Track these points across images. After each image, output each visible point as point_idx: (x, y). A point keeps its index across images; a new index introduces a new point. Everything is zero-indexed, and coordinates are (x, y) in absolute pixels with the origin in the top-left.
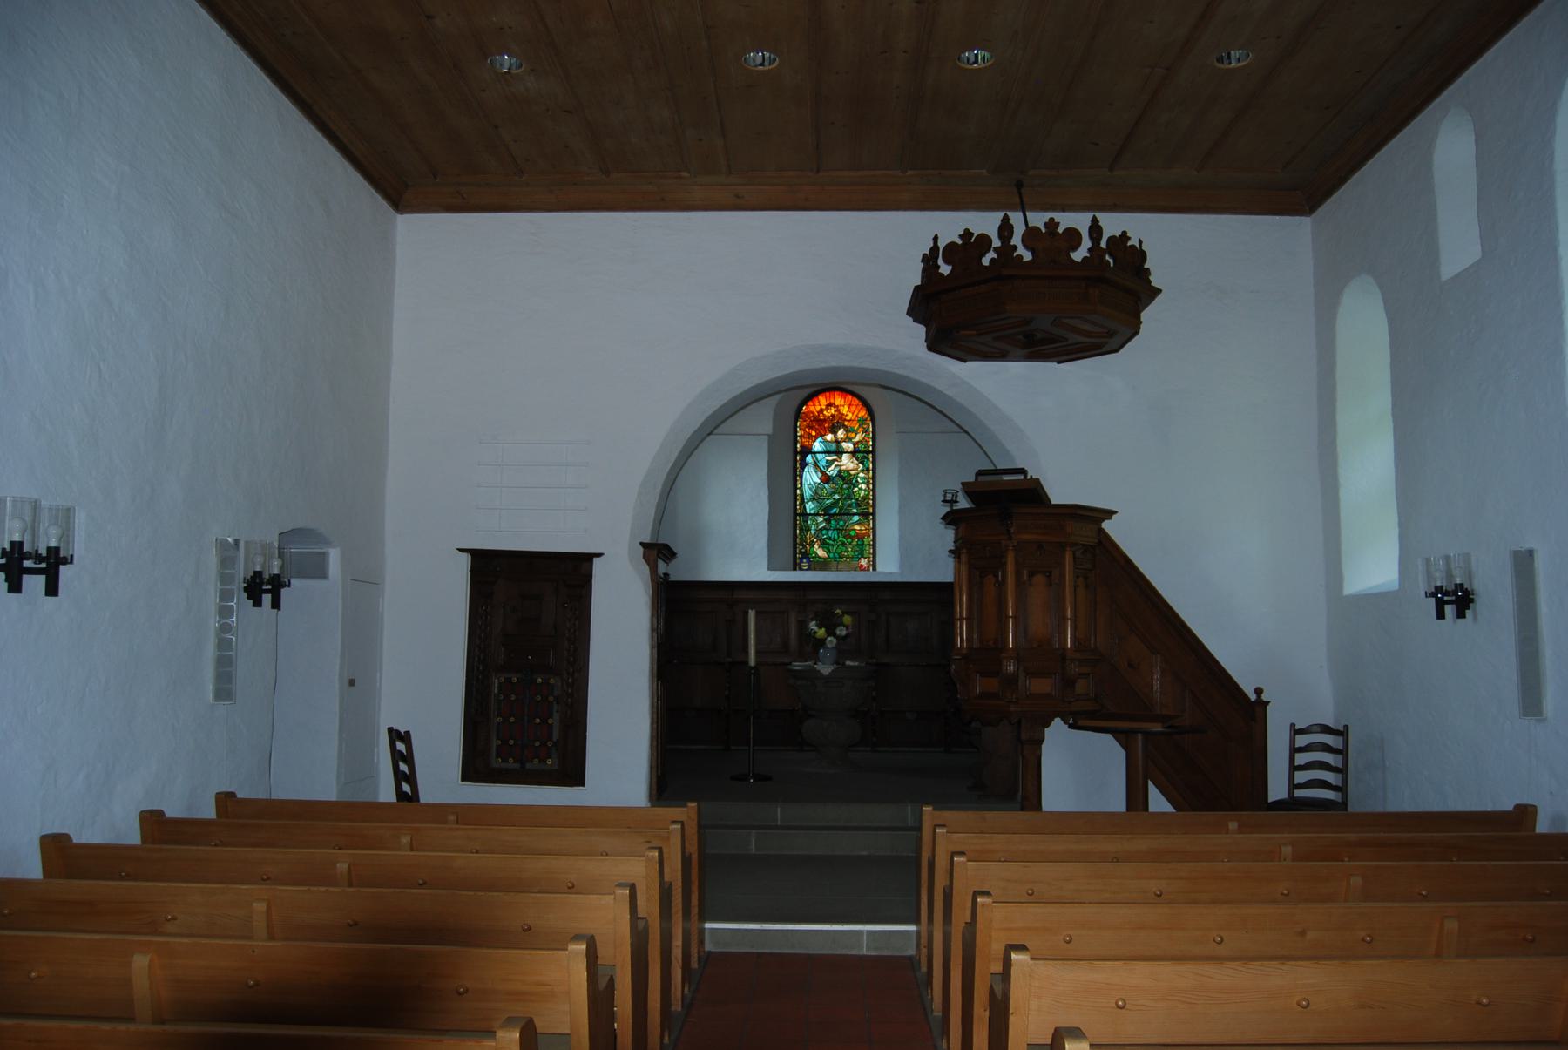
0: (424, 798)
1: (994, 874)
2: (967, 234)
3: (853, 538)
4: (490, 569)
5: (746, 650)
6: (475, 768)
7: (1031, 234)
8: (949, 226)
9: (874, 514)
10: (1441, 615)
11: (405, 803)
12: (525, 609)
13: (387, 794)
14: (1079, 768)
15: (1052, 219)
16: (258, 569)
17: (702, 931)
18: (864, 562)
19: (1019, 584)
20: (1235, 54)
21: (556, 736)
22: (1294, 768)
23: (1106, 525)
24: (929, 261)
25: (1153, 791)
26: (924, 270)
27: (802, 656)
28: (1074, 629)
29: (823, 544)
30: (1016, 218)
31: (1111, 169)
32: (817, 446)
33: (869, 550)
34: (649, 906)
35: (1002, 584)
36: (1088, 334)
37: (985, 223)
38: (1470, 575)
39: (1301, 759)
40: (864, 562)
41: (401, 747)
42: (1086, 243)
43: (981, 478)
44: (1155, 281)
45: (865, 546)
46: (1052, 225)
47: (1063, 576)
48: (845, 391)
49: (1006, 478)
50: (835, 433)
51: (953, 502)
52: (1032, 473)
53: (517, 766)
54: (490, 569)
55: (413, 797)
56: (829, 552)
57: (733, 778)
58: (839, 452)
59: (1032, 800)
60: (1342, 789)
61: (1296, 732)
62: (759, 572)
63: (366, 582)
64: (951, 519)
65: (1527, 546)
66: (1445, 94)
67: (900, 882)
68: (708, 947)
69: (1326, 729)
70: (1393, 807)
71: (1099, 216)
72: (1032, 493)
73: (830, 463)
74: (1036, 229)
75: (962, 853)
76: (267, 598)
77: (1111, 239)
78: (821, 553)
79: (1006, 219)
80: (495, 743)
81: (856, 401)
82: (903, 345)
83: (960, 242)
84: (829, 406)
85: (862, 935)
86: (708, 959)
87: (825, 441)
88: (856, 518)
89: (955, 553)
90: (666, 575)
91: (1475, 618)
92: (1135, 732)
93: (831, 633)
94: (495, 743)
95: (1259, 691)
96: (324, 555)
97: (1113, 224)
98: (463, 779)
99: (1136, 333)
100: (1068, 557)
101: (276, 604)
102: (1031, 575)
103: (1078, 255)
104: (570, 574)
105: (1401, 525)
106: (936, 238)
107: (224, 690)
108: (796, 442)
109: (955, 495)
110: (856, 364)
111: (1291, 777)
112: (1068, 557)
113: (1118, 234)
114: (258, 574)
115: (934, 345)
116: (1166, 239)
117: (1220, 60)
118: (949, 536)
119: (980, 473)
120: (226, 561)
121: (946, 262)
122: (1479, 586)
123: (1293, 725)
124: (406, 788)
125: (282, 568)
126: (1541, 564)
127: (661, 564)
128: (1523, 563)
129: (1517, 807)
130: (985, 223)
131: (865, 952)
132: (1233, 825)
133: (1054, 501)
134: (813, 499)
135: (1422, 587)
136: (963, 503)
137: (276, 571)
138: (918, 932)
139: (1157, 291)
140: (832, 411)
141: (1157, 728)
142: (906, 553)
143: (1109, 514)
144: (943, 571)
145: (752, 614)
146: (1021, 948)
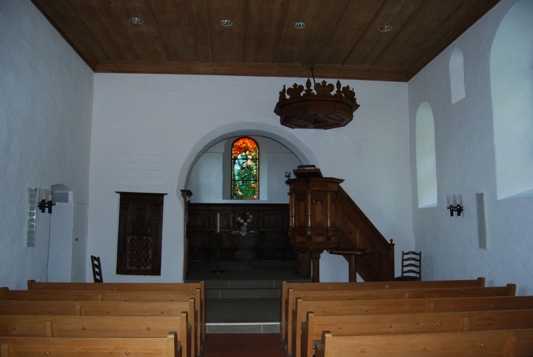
0: (105, 281)
1: (311, 305)
2: (295, 85)
3: (251, 188)
4: (128, 200)
5: (216, 228)
6: (121, 270)
7: (317, 86)
8: (289, 82)
9: (259, 180)
10: (452, 215)
11: (97, 283)
12: (139, 213)
13: (89, 278)
14: (332, 267)
15: (324, 81)
16: (44, 199)
17: (205, 326)
18: (255, 197)
19: (312, 204)
20: (386, 27)
21: (150, 257)
22: (403, 266)
23: (341, 185)
24: (282, 94)
25: (358, 276)
26: (280, 97)
27: (235, 229)
28: (330, 221)
29: (241, 191)
30: (312, 80)
31: (343, 64)
32: (239, 157)
33: (257, 193)
34: (191, 320)
35: (306, 205)
36: (335, 120)
37: (302, 81)
38: (461, 202)
39: (406, 263)
40: (255, 197)
41: (96, 262)
42: (336, 89)
43: (300, 168)
44: (358, 102)
45: (255, 191)
46: (324, 83)
47: (327, 201)
48: (249, 138)
49: (306, 168)
50: (245, 152)
51: (289, 176)
52: (317, 167)
53: (136, 268)
54: (128, 200)
55: (101, 281)
56: (243, 193)
57: (212, 272)
58: (247, 159)
59: (316, 279)
60: (419, 273)
61: (404, 254)
62: (220, 200)
63: (82, 204)
64: (289, 182)
65: (481, 192)
66: (454, 43)
67: (274, 307)
68: (207, 332)
69: (414, 253)
70: (435, 279)
71: (340, 80)
72: (317, 173)
73: (244, 163)
74: (319, 84)
75: (300, 298)
76: (47, 210)
77: (344, 88)
78: (240, 193)
79: (309, 80)
80: (128, 260)
81: (253, 142)
82: (272, 122)
83: (293, 88)
84: (244, 143)
85: (261, 326)
86: (208, 336)
87: (242, 155)
88: (253, 182)
89: (290, 194)
90: (189, 201)
91: (463, 216)
92: (352, 254)
93: (245, 221)
94: (128, 260)
95: (391, 240)
96: (67, 194)
97: (344, 83)
98: (117, 273)
99: (351, 120)
100: (329, 195)
101: (50, 212)
102: (316, 201)
103: (333, 93)
104: (156, 201)
105: (438, 185)
106: (284, 86)
107: (31, 243)
108: (232, 155)
109: (289, 174)
110: (256, 129)
111: (402, 269)
112: (329, 195)
113: (346, 86)
114: (43, 201)
115: (283, 123)
116: (361, 89)
117: (381, 29)
118: (287, 188)
119: (299, 166)
120: (32, 196)
121: (288, 94)
122: (465, 205)
123: (403, 252)
124: (98, 277)
125: (52, 198)
126: (485, 198)
127: (188, 198)
128: (480, 197)
129: (478, 278)
130: (302, 81)
131: (262, 332)
132: (387, 286)
133: (324, 176)
134: (238, 175)
135: (446, 206)
136: (293, 177)
137: (50, 200)
138: (281, 325)
139: (358, 106)
140: (245, 145)
141: (359, 253)
142: (270, 194)
143: (342, 181)
144: (285, 199)
145: (218, 215)
146: (329, 332)
